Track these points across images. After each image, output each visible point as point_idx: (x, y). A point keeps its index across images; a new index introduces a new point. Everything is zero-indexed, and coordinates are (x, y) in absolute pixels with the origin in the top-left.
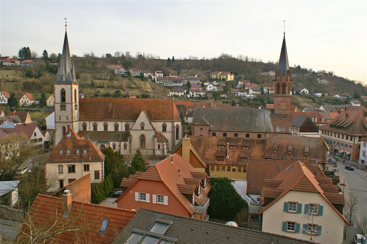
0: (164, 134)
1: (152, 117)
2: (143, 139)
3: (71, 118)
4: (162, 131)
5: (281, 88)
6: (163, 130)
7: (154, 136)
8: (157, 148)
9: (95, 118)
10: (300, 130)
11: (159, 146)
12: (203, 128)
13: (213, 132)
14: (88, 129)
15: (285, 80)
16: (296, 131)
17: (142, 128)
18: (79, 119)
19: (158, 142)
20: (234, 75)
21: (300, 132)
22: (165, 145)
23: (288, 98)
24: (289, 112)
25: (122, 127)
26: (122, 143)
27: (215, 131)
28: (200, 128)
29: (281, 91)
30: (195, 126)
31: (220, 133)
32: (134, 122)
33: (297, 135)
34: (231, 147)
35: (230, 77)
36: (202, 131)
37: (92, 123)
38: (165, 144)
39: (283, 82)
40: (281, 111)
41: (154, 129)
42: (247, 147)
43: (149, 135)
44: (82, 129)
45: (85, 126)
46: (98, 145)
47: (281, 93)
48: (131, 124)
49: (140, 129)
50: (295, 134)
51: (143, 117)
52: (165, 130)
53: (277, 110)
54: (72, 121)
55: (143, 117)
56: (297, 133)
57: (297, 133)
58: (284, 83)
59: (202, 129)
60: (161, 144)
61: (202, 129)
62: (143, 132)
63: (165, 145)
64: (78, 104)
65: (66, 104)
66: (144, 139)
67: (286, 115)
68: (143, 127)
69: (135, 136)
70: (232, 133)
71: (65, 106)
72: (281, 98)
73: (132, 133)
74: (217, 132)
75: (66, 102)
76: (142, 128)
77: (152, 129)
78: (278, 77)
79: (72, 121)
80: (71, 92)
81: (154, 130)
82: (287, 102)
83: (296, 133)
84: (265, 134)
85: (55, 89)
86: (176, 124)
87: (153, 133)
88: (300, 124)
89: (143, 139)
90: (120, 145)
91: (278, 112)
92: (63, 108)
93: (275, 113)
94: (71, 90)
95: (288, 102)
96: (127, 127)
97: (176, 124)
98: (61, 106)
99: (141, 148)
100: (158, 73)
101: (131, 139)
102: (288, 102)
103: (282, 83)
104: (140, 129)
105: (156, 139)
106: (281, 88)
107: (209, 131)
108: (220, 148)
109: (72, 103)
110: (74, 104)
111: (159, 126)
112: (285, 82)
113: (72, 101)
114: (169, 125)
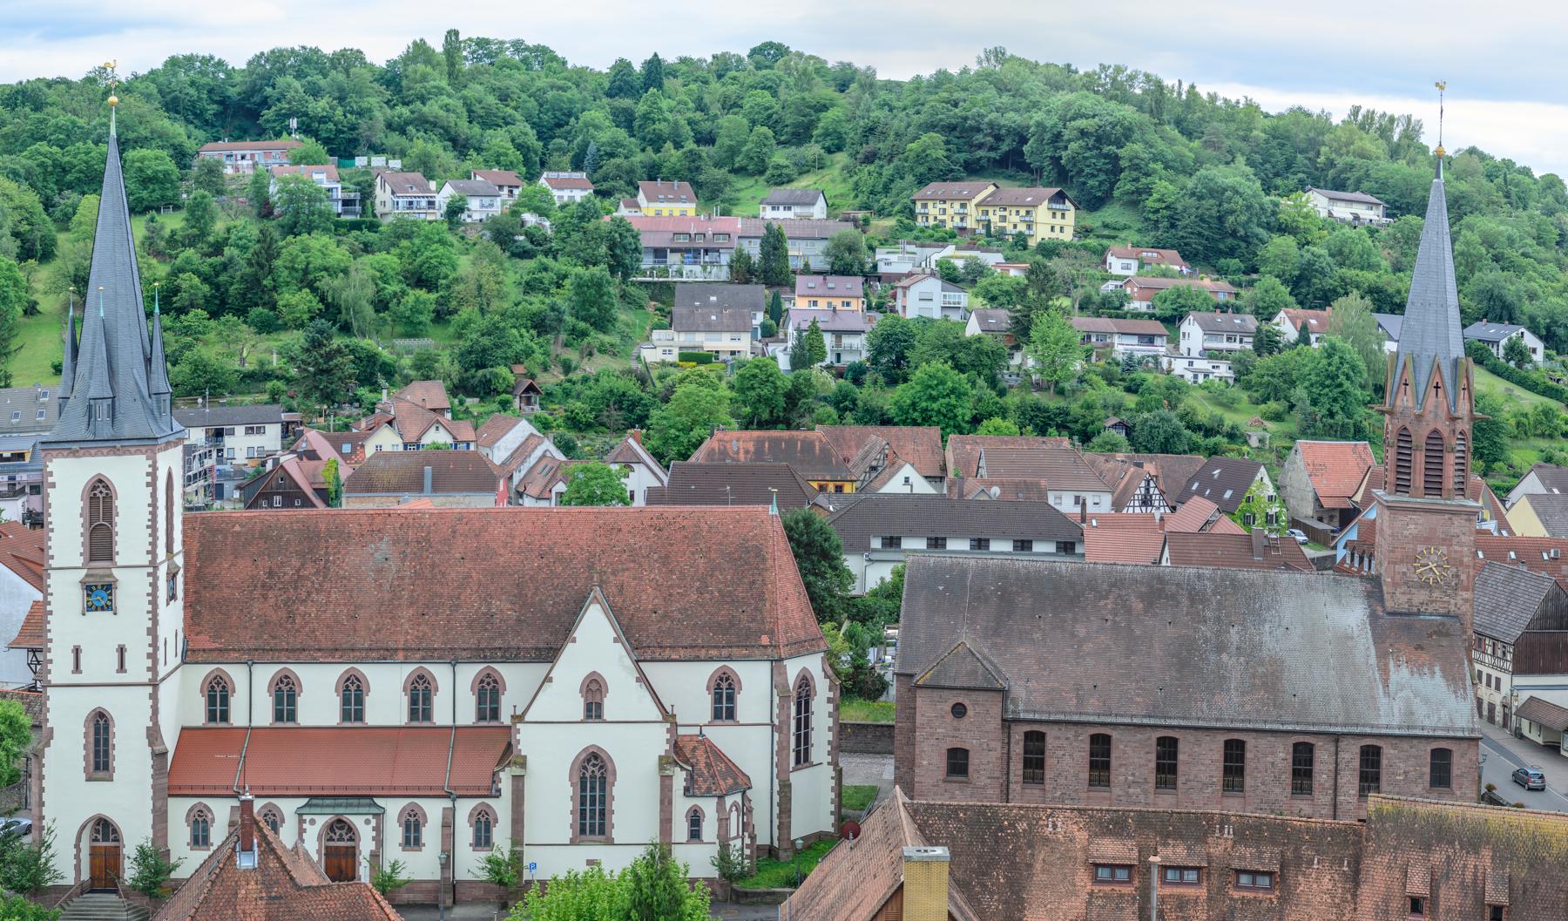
0: (721, 736)
1: (644, 642)
2: (593, 780)
3: (149, 669)
4: (706, 714)
5: (1419, 460)
6: (717, 715)
7: (664, 762)
8: (681, 829)
9: (287, 643)
10: (1515, 661)
11: (695, 820)
12: (966, 703)
13: (1028, 728)
14: (238, 718)
15: (1443, 414)
16: (1493, 666)
17: (594, 711)
18: (185, 653)
19: (687, 792)
20: (1077, 208)
21: (1518, 671)
22: (734, 815)
23: (1457, 520)
24: (1466, 600)
25: (455, 699)
26: (465, 808)
27: (1041, 722)
28: (948, 707)
29: (1418, 479)
30: (919, 693)
31: (1070, 732)
32: (540, 670)
33: (1498, 688)
34: (1170, 875)
35: (1054, 221)
36: (964, 723)
37: (265, 674)
38: (735, 804)
39: (1432, 427)
40: (1420, 596)
41: (668, 717)
42: (1264, 873)
43: (636, 754)
44: (199, 718)
45: (218, 696)
46: (313, 822)
47: (1422, 489)
48: (516, 678)
49: (580, 715)
50: (1489, 684)
51: (595, 641)
52: (731, 714)
53: (1395, 585)
54: (150, 675)
55: (595, 641)
56: (1499, 675)
57: (1498, 680)
58: (1436, 431)
59: (959, 711)
60: (709, 806)
61: (959, 711)
62: (594, 735)
63: (734, 815)
64: (179, 560)
65: (115, 572)
66: (603, 779)
67: (1447, 615)
68: (599, 706)
69: (549, 754)
70: (1140, 736)
71: (109, 588)
72: (1420, 518)
73: (528, 740)
74: (1056, 727)
75: (119, 560)
76: (594, 711)
77: (656, 714)
78: (1401, 395)
79: (150, 675)
80: (150, 501)
81: (665, 720)
82: (1455, 541)
83: (1495, 674)
84: (1337, 741)
85: (53, 485)
86: (793, 669)
87: (657, 741)
88: (1514, 624)
89: (593, 780)
90: (448, 825)
91: (1403, 599)
92: (100, 598)
93: (1389, 604)
94: (152, 484)
95: (1460, 544)
96: (489, 694)
97: (793, 669)
98: (89, 589)
99: (583, 831)
100: (562, 189)
101: (518, 780)
102: (1460, 544)
103: (1426, 433)
104: (579, 712)
105: (679, 778)
106: (1419, 460)
107: (1007, 723)
108: (1103, 882)
109: (154, 565)
110: (162, 572)
111: (687, 685)
112: (1444, 429)
113: (153, 552)
114: (754, 678)
